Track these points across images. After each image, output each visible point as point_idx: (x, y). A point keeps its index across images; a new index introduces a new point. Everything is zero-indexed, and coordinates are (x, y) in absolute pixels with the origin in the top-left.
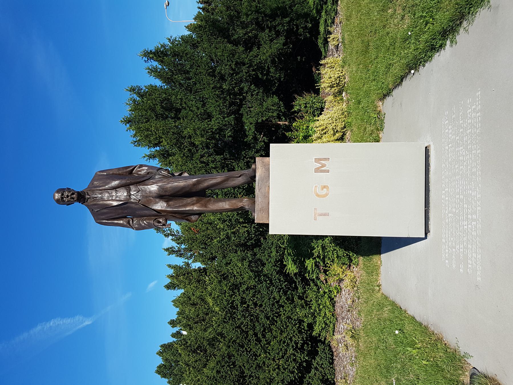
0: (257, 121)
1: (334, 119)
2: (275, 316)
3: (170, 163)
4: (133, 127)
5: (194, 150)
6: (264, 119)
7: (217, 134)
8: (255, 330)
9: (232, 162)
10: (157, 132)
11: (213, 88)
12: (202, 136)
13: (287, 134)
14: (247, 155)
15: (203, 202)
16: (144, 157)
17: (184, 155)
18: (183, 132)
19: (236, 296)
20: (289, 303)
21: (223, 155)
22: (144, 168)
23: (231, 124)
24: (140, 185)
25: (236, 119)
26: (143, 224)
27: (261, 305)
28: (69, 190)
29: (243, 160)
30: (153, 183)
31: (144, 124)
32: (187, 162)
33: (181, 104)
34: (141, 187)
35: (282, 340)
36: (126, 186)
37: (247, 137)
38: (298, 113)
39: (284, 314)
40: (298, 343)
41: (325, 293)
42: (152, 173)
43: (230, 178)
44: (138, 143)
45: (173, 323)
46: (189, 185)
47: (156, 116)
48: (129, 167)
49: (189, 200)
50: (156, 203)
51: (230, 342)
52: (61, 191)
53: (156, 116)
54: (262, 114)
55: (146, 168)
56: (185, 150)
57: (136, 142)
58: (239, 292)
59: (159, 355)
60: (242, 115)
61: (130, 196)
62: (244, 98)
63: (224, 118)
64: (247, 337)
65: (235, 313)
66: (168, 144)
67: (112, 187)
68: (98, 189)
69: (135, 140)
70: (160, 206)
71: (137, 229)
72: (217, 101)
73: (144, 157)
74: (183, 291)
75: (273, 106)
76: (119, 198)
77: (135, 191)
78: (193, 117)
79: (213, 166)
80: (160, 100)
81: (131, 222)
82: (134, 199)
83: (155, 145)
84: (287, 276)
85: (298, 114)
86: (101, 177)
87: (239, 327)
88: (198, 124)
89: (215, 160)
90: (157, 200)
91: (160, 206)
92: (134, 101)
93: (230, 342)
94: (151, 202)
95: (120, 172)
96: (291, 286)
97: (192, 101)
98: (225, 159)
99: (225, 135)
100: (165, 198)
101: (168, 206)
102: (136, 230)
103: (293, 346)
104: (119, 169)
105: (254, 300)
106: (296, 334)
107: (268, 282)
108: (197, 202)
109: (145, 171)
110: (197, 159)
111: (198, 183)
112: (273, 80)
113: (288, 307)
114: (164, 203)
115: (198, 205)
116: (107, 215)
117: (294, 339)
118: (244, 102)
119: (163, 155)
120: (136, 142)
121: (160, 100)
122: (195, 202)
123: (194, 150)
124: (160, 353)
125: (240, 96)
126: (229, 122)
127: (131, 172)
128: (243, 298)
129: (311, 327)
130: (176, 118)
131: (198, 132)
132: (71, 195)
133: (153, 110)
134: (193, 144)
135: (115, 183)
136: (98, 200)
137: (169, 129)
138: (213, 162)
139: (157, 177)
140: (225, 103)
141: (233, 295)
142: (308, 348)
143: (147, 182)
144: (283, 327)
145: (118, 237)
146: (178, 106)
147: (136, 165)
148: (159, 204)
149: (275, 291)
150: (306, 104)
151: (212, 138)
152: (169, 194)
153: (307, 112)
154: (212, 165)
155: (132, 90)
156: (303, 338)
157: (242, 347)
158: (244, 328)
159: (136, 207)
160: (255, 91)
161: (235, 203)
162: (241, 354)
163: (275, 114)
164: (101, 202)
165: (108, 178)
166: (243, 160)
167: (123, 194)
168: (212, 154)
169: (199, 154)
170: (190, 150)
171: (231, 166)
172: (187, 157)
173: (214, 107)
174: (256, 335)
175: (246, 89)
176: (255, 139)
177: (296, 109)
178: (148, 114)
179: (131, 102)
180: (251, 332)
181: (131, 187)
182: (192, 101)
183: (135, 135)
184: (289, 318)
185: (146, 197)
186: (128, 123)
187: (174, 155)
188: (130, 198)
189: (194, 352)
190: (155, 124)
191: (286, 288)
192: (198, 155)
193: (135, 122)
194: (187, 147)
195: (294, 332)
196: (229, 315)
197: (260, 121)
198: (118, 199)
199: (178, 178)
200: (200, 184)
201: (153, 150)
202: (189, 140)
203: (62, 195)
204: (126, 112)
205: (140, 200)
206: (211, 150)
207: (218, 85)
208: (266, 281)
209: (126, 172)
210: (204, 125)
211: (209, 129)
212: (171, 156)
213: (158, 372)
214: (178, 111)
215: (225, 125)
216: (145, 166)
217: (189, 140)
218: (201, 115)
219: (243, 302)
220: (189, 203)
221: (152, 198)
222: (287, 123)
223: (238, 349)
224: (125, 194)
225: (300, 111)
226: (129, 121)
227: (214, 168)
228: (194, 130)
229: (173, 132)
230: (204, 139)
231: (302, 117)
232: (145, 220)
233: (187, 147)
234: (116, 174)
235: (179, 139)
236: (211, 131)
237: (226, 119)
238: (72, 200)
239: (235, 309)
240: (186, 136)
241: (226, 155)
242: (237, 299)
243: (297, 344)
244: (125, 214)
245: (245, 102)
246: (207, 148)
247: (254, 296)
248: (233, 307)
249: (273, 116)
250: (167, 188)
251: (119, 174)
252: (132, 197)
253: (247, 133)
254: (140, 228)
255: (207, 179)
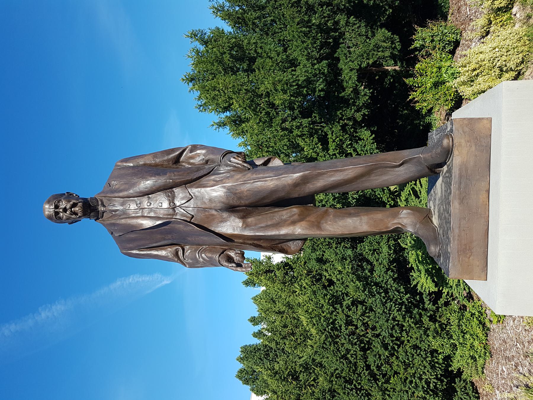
0: (360, 66)
1: (504, 50)
2: (397, 344)
3: (243, 132)
4: (196, 86)
5: (273, 113)
6: (371, 61)
7: (304, 87)
8: (367, 361)
9: (323, 127)
10: (226, 91)
11: (298, 24)
12: (285, 92)
13: (407, 81)
14: (343, 116)
15: (312, 218)
16: (213, 125)
17: (260, 120)
18: (259, 88)
19: (338, 313)
20: (417, 328)
21: (311, 117)
22: (198, 152)
23: (323, 73)
24: (191, 187)
25: (329, 65)
26: (201, 260)
27: (374, 328)
28: (69, 196)
29: (339, 122)
30: (216, 183)
31: (209, 82)
32: (264, 130)
33: (255, 51)
34: (194, 191)
35: (407, 378)
36: (167, 189)
37: (344, 90)
38: (420, 51)
39: (408, 341)
40: (430, 382)
41: (473, 315)
42: (213, 161)
43: (376, 169)
44: (203, 107)
45: (254, 321)
46: (284, 186)
47: (225, 70)
48: (173, 150)
49: (285, 213)
50: (224, 221)
51: (332, 376)
52: (56, 199)
53: (224, 70)
54: (368, 55)
55: (204, 151)
56: (261, 113)
57: (201, 106)
58: (341, 307)
59: (240, 361)
60: (338, 59)
61: (173, 209)
62: (342, 34)
63: (313, 65)
64: (356, 369)
65: (338, 336)
66: (240, 106)
67: (141, 192)
68: (117, 195)
69: (200, 103)
70: (231, 226)
71: (191, 266)
72: (303, 42)
73: (213, 125)
74: (264, 288)
75: (384, 42)
76: (155, 213)
77: (182, 199)
78: (272, 66)
79: (299, 133)
80: (229, 46)
81: (180, 253)
82: (183, 215)
83: (226, 109)
84: (413, 291)
85: (420, 52)
86: (122, 172)
87: (344, 357)
88: (279, 75)
89: (301, 125)
90: (225, 215)
91: (231, 226)
92: (198, 52)
93: (332, 376)
94: (214, 219)
95: (158, 160)
96: (414, 299)
97: (270, 44)
98: (313, 123)
99: (315, 88)
100: (238, 211)
101: (246, 226)
102: (190, 267)
103: (423, 387)
104: (155, 155)
105: (364, 320)
106: (428, 371)
107: (383, 294)
108: (302, 218)
109: (202, 157)
110: (278, 125)
111: (305, 180)
112: (383, 6)
113: (416, 333)
114: (237, 220)
115: (303, 223)
116: (137, 241)
117: (424, 377)
118: (341, 41)
119: (234, 121)
120: (201, 106)
121: (229, 46)
122: (296, 217)
123: (273, 113)
124: (241, 360)
125: (335, 32)
126: (320, 70)
127: (177, 160)
128: (349, 316)
129: (448, 359)
130: (250, 70)
131: (279, 88)
132: (71, 208)
133: (221, 62)
134: (272, 105)
135: (147, 183)
136: (119, 217)
137: (241, 85)
138: (298, 127)
139: (223, 169)
140: (315, 43)
141: (334, 311)
142: (442, 386)
143: (204, 180)
144: (408, 359)
145: (163, 276)
146: (253, 54)
147: (185, 146)
148: (228, 223)
149: (395, 308)
150: (432, 36)
151: (297, 94)
152: (247, 202)
153: (434, 48)
154: (296, 132)
155: (194, 35)
156: (437, 375)
157: (350, 382)
158: (352, 359)
159: (185, 229)
160: (355, 24)
161: (382, 220)
162: (348, 393)
163: (387, 54)
164: (123, 221)
165: (135, 175)
166: (339, 122)
167: (162, 203)
168: (296, 118)
169: (280, 118)
170: (268, 114)
171: (322, 131)
172: (264, 123)
173: (300, 50)
174: (368, 367)
175: (342, 23)
176: (356, 91)
177: (417, 44)
178: (215, 68)
179: (194, 53)
180: (361, 364)
181: (176, 190)
182: (271, 45)
183: (200, 97)
184: (415, 347)
185: (205, 209)
186: (191, 81)
187: (248, 120)
188: (175, 214)
189: (285, 379)
190: (223, 81)
191: (409, 302)
192: (278, 120)
193: (199, 80)
194: (264, 109)
195: (425, 367)
196: (330, 339)
197: (364, 65)
198: (152, 214)
199: (264, 171)
200: (308, 182)
201: (223, 116)
202: (266, 99)
203: (57, 207)
204: (188, 67)
205: (193, 216)
206: (297, 112)
207: (306, 18)
208: (379, 293)
209: (168, 160)
210: (287, 76)
211: (293, 82)
212: (244, 122)
213: (239, 377)
214: (252, 60)
215: (315, 75)
216: (202, 147)
217: (266, 99)
218: (283, 63)
219: (349, 323)
220: (285, 221)
221: (214, 212)
222: (397, 68)
223: (345, 386)
224: (166, 205)
225: (423, 47)
226: (192, 80)
227: (300, 136)
228: (274, 84)
229: (245, 90)
230: (286, 97)
231: (429, 55)
232: (205, 251)
233: (264, 109)
234: (150, 165)
235: (254, 99)
236: (297, 85)
237: (316, 67)
238: (73, 216)
239: (336, 329)
240: (262, 94)
241: (315, 117)
242: (341, 319)
243: (428, 383)
244: (171, 237)
245: (343, 39)
246: (290, 110)
247: (363, 314)
248: (334, 329)
249: (384, 57)
250: (242, 192)
251: (156, 165)
252: (179, 210)
253: (345, 84)
254: (194, 264)
255: (324, 174)
